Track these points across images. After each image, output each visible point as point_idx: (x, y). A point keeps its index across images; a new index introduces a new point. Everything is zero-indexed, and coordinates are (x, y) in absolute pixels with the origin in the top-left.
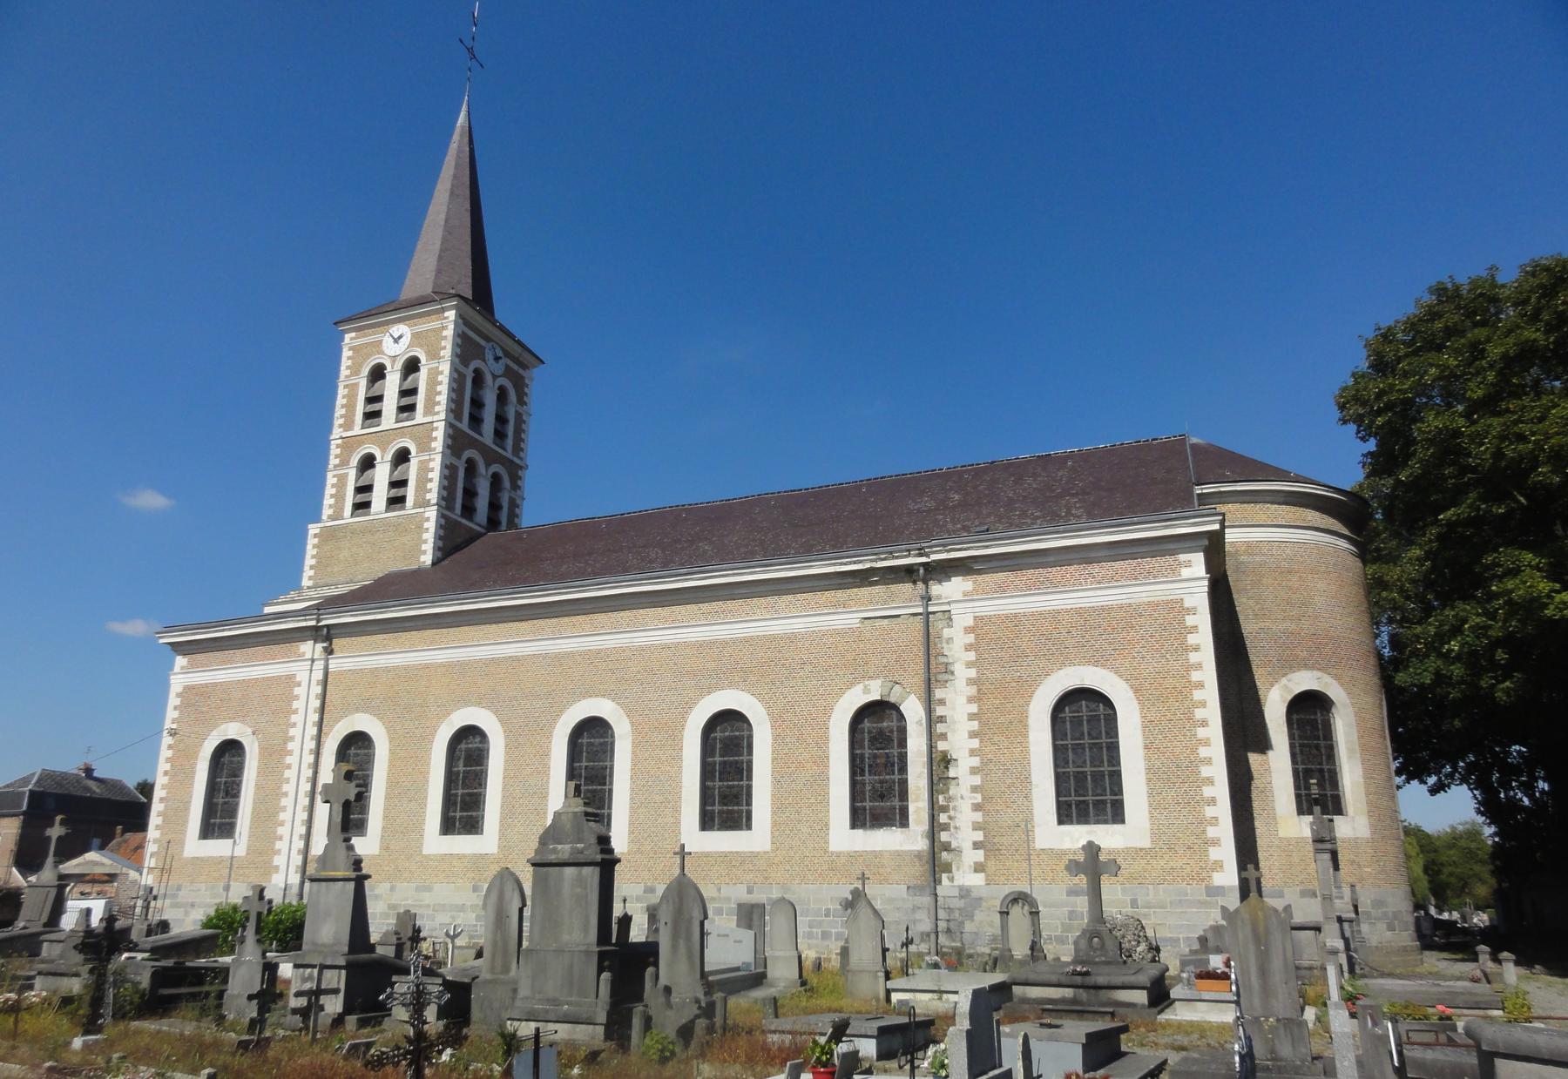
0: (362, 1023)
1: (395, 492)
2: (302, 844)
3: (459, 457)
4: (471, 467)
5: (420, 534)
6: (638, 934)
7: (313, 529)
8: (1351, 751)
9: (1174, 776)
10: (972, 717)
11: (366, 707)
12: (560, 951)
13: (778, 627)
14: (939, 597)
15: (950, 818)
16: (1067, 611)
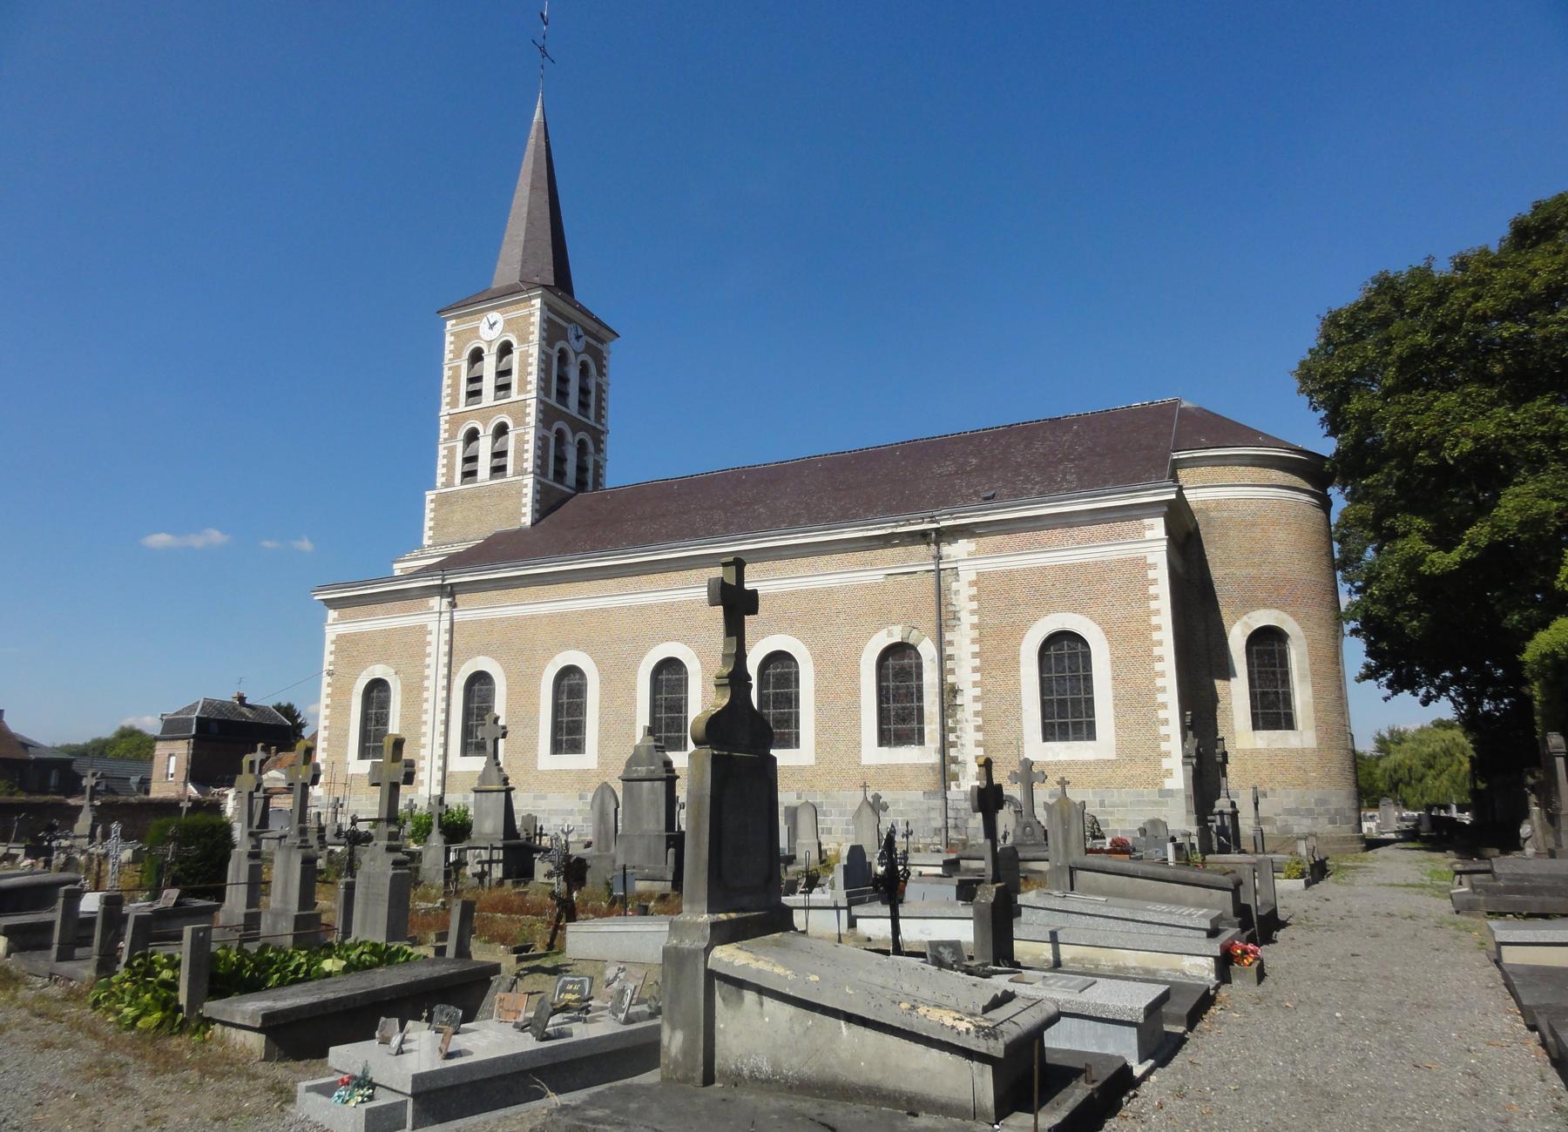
0: (517, 884)
1: (497, 462)
2: (440, 763)
3: (549, 429)
4: (560, 435)
8: (1302, 677)
9: (1135, 701)
10: (975, 655)
11: (485, 651)
12: (642, 836)
14: (948, 556)
16: (1052, 568)
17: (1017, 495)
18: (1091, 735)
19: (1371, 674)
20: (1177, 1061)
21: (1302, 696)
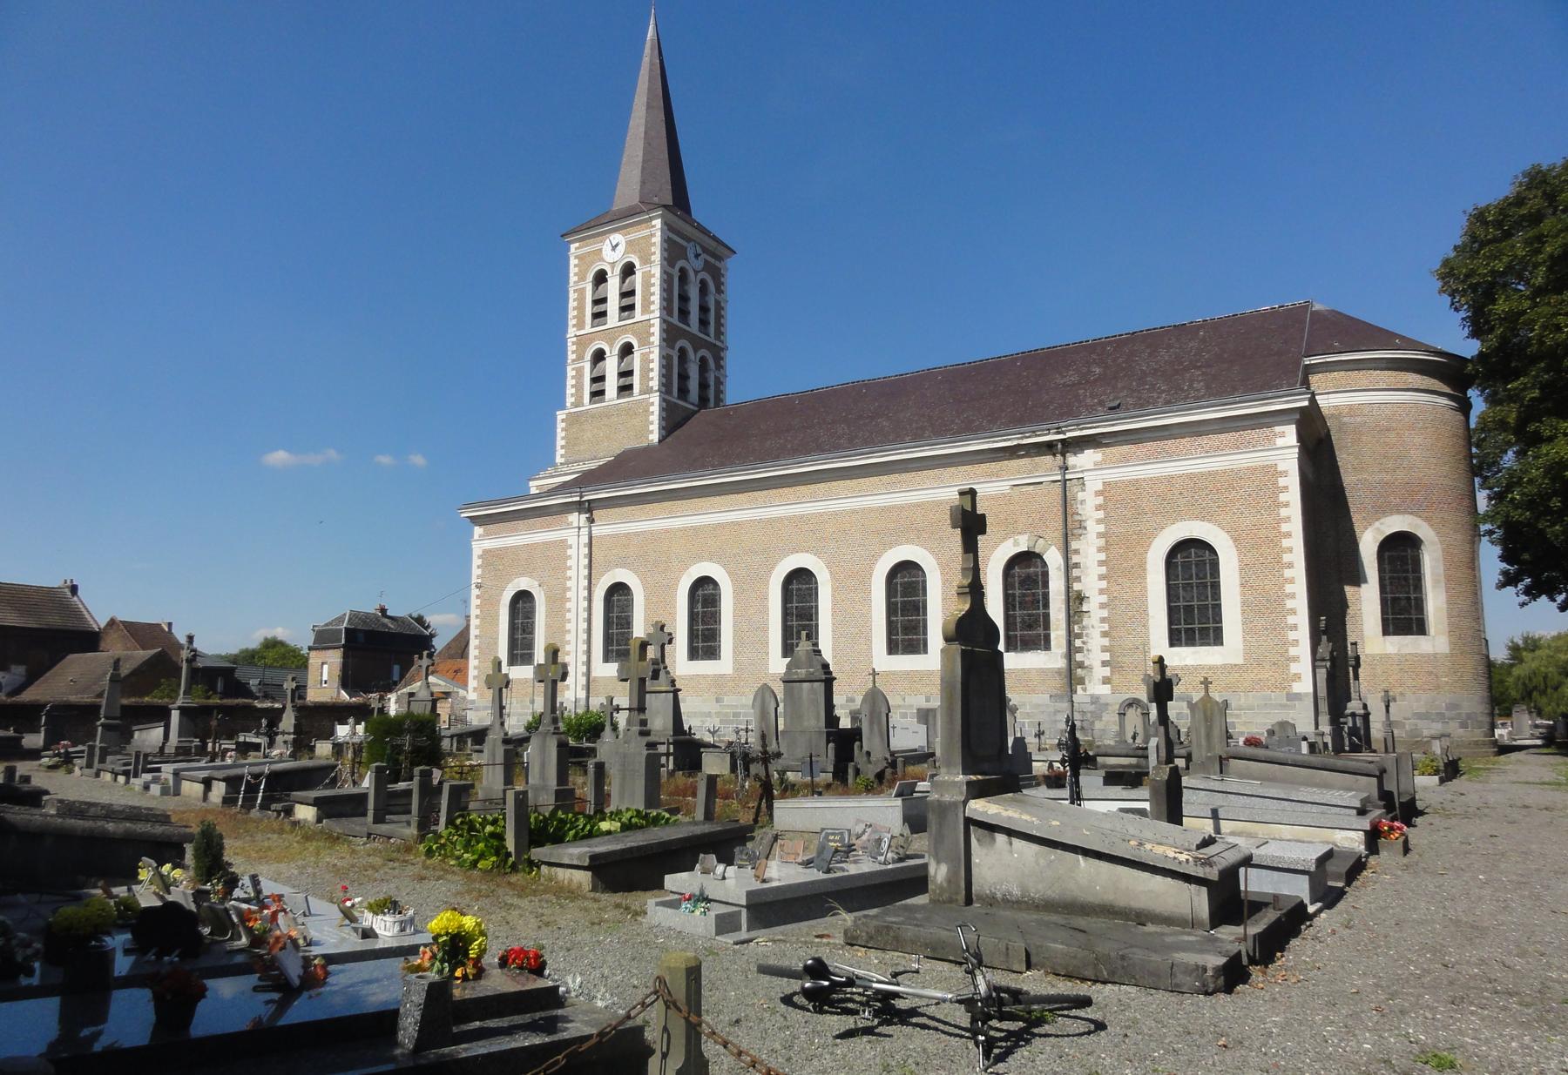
2: (584, 669)
4: (682, 352)
6: (845, 723)
7: (561, 415)
8: (1436, 582)
9: (1264, 607)
10: (1101, 563)
17: (1143, 405)
18: (1218, 639)
19: (1509, 580)
20: (1341, 905)
21: (1435, 602)
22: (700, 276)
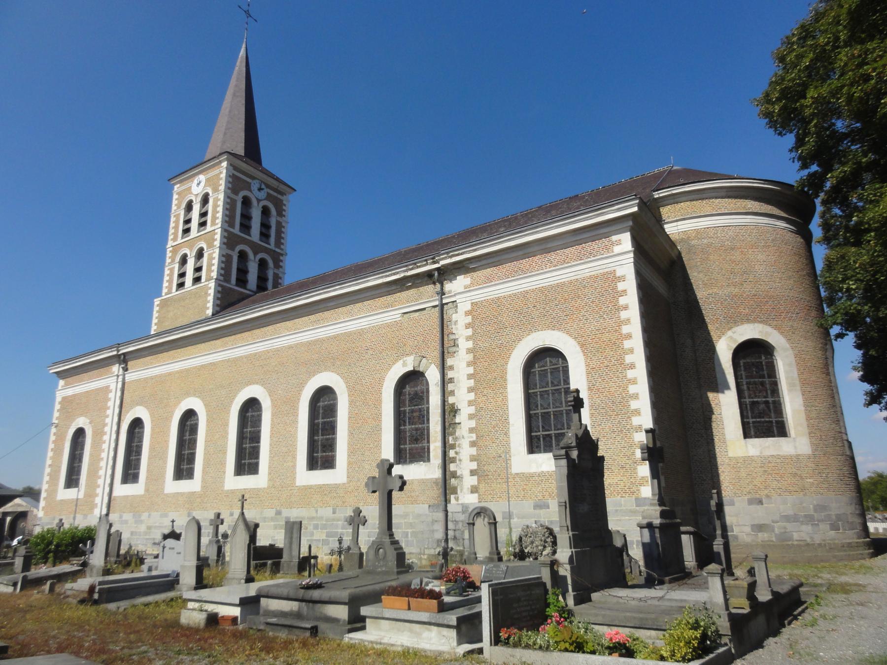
3: (233, 250)
4: (243, 256)
5: (206, 297)
8: (791, 386)
10: (470, 377)
13: (353, 326)
14: (450, 292)
15: (456, 453)
16: (533, 291)
21: (793, 405)
22: (262, 203)
